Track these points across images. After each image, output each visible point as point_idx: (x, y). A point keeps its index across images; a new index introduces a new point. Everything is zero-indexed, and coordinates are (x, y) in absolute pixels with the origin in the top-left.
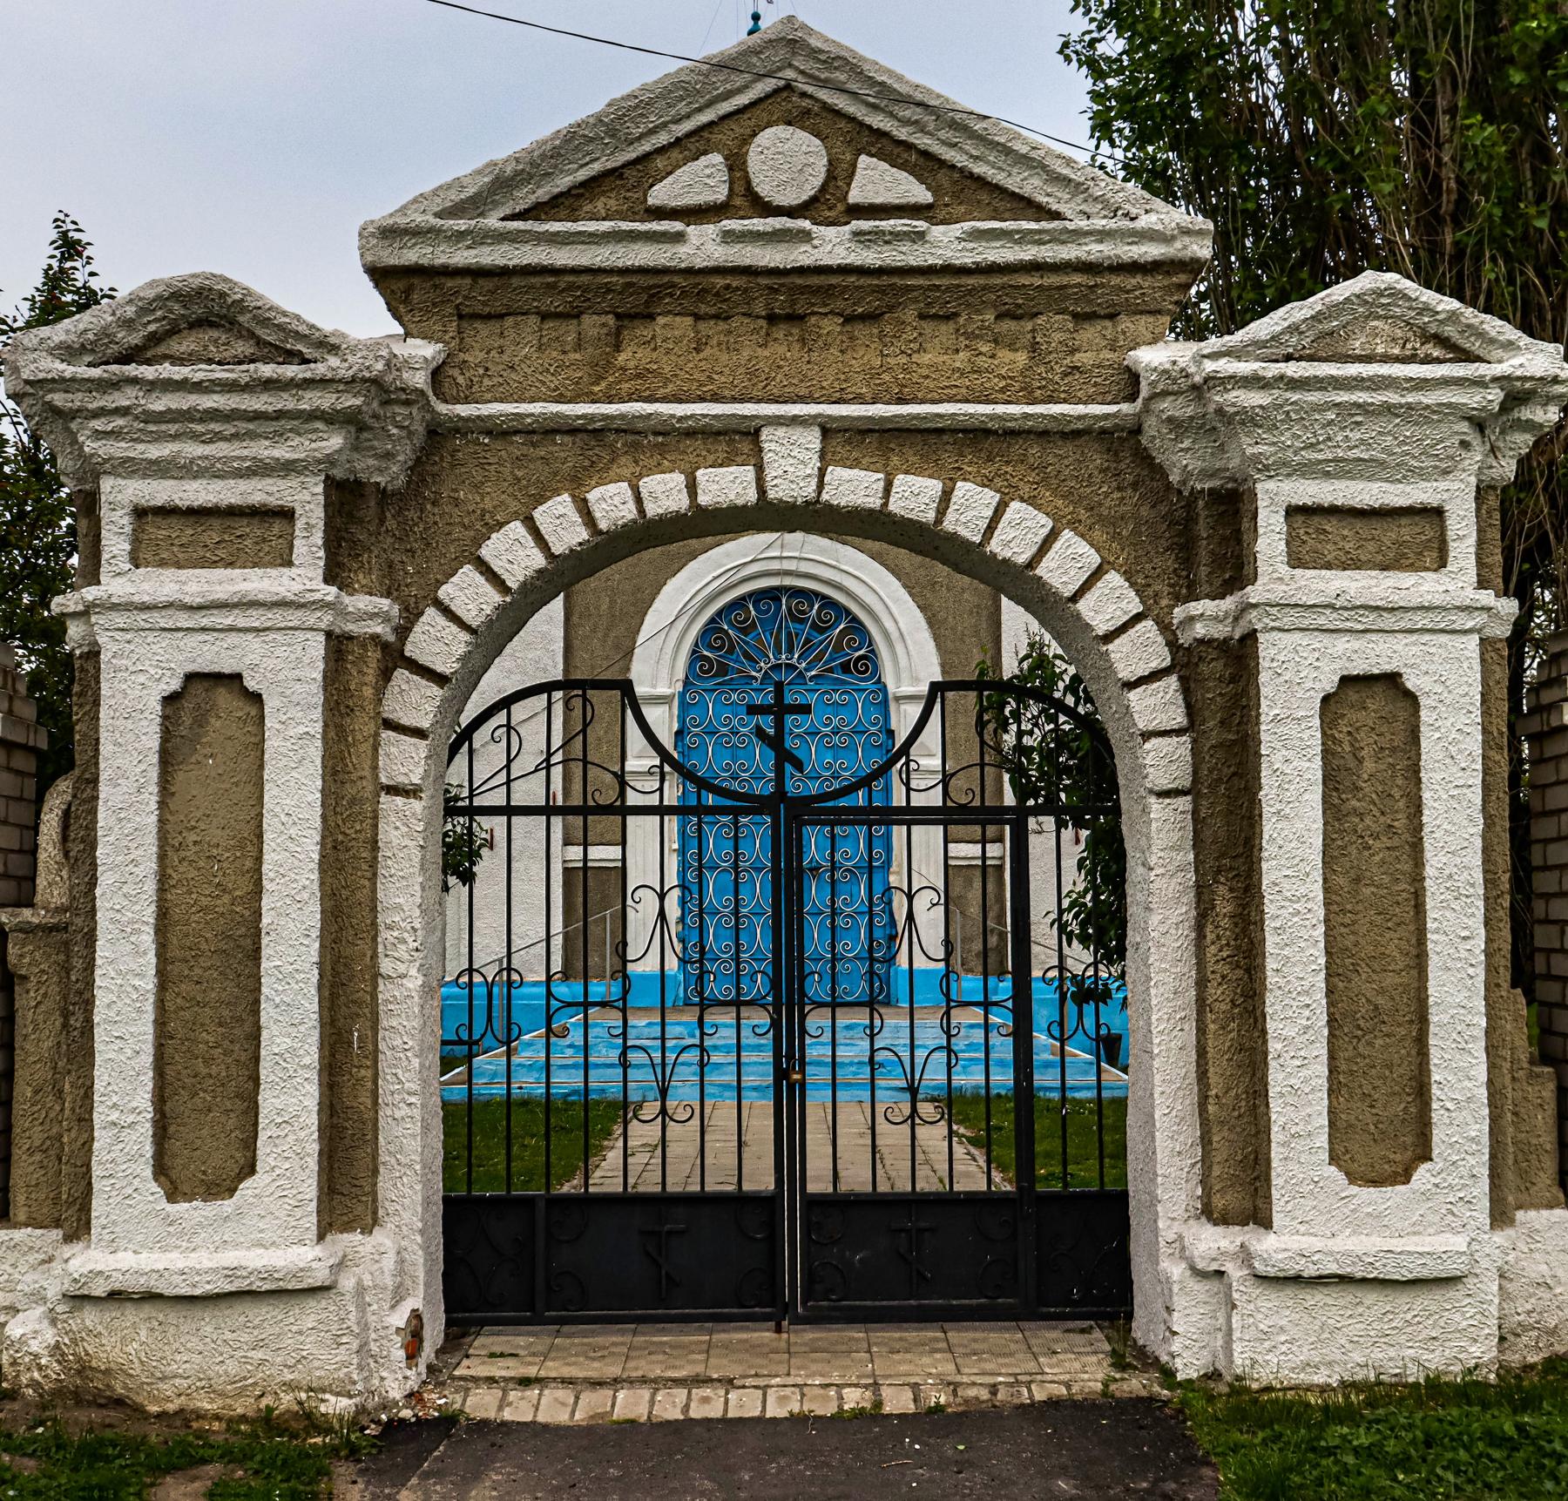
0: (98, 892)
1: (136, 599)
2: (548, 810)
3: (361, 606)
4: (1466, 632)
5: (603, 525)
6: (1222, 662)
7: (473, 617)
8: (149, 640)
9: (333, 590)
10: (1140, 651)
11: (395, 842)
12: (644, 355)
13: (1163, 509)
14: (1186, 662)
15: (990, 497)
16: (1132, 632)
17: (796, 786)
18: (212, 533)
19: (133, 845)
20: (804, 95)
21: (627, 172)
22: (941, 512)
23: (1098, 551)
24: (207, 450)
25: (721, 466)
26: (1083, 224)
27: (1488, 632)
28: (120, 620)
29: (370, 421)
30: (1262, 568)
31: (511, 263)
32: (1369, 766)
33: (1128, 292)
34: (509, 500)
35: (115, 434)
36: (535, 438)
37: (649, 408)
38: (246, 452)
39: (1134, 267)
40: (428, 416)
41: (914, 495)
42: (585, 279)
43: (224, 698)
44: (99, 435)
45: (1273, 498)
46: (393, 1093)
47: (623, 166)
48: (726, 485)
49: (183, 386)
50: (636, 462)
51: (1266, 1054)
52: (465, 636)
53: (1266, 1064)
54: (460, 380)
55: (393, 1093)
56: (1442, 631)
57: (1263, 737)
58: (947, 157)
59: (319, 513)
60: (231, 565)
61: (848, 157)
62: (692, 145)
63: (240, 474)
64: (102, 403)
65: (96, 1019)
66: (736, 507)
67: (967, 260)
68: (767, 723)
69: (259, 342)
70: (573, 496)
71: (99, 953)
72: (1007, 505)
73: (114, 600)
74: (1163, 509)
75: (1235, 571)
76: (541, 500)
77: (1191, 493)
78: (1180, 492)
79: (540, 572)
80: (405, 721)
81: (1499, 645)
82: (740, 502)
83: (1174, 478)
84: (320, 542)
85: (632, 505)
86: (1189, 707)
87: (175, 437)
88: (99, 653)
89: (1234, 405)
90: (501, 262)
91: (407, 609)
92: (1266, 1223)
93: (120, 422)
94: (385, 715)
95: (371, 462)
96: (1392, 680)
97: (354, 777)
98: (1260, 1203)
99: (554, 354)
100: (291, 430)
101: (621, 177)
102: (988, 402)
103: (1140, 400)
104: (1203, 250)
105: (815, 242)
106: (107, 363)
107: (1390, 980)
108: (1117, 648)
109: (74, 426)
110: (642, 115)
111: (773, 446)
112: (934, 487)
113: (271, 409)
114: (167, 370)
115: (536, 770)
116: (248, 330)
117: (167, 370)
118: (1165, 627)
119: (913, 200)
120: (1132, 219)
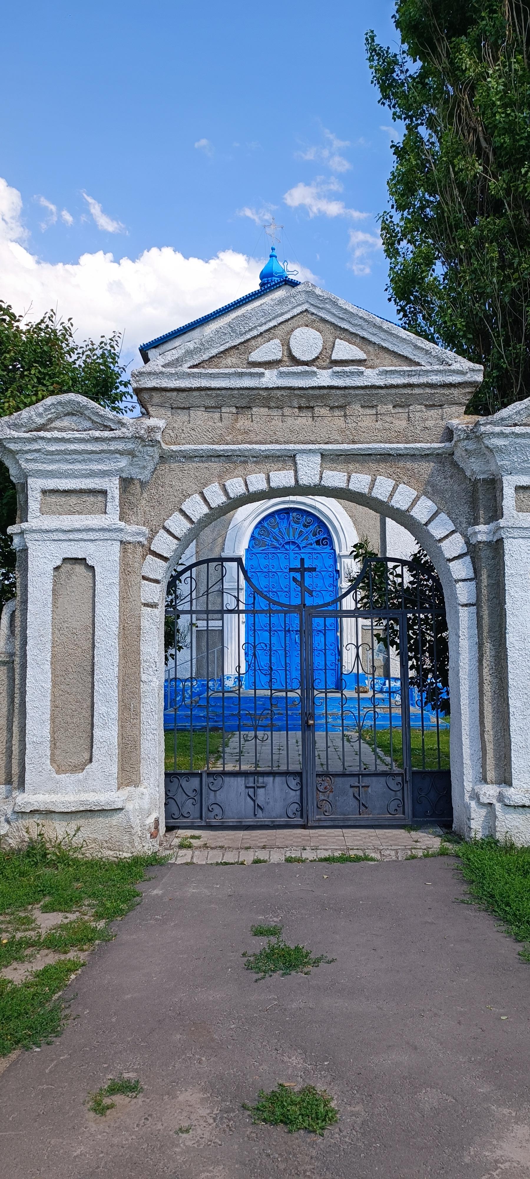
0: (27, 648)
1: (43, 528)
3: (134, 530)
5: (232, 495)
6: (489, 551)
8: (48, 544)
9: (123, 523)
10: (454, 546)
13: (463, 486)
14: (472, 550)
15: (391, 483)
16: (450, 538)
17: (309, 601)
18: (73, 500)
19: (41, 629)
20: (313, 314)
21: (240, 347)
22: (371, 489)
23: (436, 504)
24: (71, 467)
25: (279, 470)
26: (429, 368)
28: (36, 536)
29: (137, 453)
30: (505, 512)
31: (193, 386)
33: (448, 396)
34: (193, 486)
35: (34, 460)
36: (204, 459)
37: (250, 447)
38: (87, 467)
39: (451, 385)
40: (160, 451)
41: (360, 482)
42: (223, 392)
43: (80, 569)
46: (146, 729)
47: (239, 344)
49: (63, 440)
50: (245, 469)
51: (509, 713)
53: (509, 717)
54: (172, 434)
55: (146, 729)
57: (506, 582)
58: (373, 340)
59: (117, 492)
60: (80, 513)
61: (331, 339)
62: (267, 334)
63: (86, 476)
64: (29, 448)
65: (27, 700)
66: (286, 487)
67: (381, 383)
68: (298, 576)
69: (93, 422)
70: (219, 483)
71: (28, 673)
72: (398, 486)
73: (34, 528)
74: (463, 486)
75: (495, 513)
76: (205, 485)
77: (475, 480)
78: (470, 479)
79: (206, 515)
80: (151, 577)
82: (288, 485)
83: (468, 474)
84: (118, 504)
85: (244, 487)
86: (475, 569)
87: (58, 461)
88: (27, 549)
89: (493, 444)
90: (190, 386)
91: (151, 530)
92: (510, 785)
93: (37, 455)
94: (143, 574)
95: (137, 470)
97: (131, 600)
98: (506, 775)
99: (210, 423)
100: (106, 458)
101: (238, 349)
103: (453, 442)
105: (318, 376)
106: (32, 431)
108: (444, 545)
109: (17, 457)
110: (246, 323)
111: (301, 462)
112: (368, 478)
113: (98, 449)
114: (56, 434)
115: (203, 596)
116: (88, 417)
117: (56, 434)
118: (465, 536)
119: (358, 358)
120: (450, 365)
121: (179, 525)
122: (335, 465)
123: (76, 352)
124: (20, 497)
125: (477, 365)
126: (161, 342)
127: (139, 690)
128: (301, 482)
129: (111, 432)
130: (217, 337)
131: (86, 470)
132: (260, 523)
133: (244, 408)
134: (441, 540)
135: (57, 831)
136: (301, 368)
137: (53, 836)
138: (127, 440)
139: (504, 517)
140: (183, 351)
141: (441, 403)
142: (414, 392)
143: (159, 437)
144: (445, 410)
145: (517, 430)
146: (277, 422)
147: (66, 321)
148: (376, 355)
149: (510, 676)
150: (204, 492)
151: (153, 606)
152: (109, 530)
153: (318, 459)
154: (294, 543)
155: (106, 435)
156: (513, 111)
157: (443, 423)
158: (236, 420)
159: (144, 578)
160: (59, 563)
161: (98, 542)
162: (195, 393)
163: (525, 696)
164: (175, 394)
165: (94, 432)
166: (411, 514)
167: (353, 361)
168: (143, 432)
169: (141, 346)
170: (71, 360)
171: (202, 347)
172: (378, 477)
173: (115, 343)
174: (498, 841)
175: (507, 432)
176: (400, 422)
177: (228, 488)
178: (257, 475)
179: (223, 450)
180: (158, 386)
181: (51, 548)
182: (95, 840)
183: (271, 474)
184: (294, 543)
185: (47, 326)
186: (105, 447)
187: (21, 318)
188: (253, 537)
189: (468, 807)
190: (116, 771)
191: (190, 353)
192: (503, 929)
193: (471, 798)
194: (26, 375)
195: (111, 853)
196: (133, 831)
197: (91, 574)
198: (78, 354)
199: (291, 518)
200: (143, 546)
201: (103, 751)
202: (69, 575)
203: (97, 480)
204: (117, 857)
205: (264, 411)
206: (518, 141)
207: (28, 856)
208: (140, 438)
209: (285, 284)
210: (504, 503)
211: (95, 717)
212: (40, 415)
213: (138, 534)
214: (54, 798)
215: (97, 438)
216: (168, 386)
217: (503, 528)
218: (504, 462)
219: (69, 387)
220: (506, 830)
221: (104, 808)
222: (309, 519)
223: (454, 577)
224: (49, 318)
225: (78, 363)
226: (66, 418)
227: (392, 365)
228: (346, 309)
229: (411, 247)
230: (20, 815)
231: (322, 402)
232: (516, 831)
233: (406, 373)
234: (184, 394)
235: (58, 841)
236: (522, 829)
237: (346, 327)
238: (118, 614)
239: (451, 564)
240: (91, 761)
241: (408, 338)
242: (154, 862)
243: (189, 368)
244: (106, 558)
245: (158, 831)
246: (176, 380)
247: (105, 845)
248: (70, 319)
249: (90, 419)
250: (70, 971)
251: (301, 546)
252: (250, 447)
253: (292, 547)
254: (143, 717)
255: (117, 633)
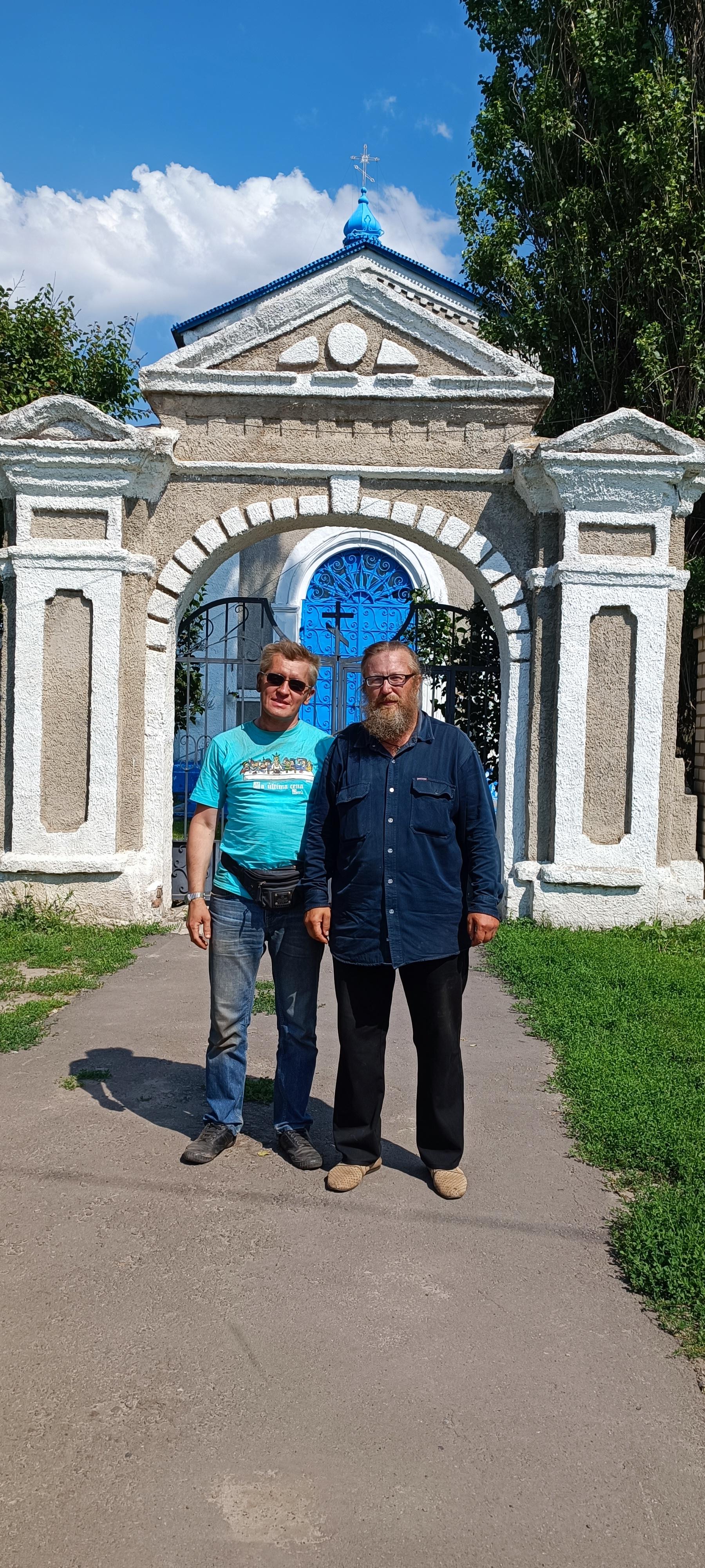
0: (15, 690)
2: (225, 661)
3: (138, 559)
4: (661, 587)
5: (254, 523)
7: (191, 566)
10: (508, 591)
11: (153, 672)
12: (276, 437)
16: (505, 582)
18: (69, 522)
19: (31, 669)
20: (357, 307)
26: (490, 378)
27: (673, 587)
30: (566, 552)
32: (612, 649)
34: (210, 509)
35: (24, 474)
43: (76, 602)
44: (16, 474)
45: (573, 520)
47: (268, 342)
48: (314, 503)
52: (188, 575)
54: (187, 448)
56: (651, 586)
57: (562, 634)
60: (76, 537)
61: (378, 339)
65: (14, 748)
66: (318, 515)
68: (332, 621)
69: (92, 430)
73: (23, 553)
75: (555, 554)
76: (224, 509)
80: (159, 615)
81: (680, 593)
83: (530, 507)
84: (120, 528)
85: (268, 513)
91: (160, 561)
94: (149, 612)
96: (624, 610)
101: (266, 347)
102: (442, 467)
104: (550, 393)
105: (360, 384)
106: (20, 438)
107: (616, 750)
108: (497, 589)
110: (277, 316)
112: (414, 508)
114: (49, 443)
117: (49, 443)
119: (408, 363)
121: (192, 557)
122: (376, 491)
123: (79, 339)
124: (7, 516)
125: (547, 377)
126: (201, 322)
127: (142, 744)
128: (335, 510)
129: (113, 443)
130: (242, 331)
131: (84, 487)
132: (322, 566)
133: (272, 419)
134: (494, 584)
135: (48, 894)
136: (338, 374)
137: (42, 899)
138: (131, 453)
139: (564, 559)
140: (201, 347)
141: (503, 422)
142: (471, 407)
143: (168, 450)
144: (507, 430)
145: (583, 456)
146: (311, 438)
147: (66, 301)
148: (430, 360)
149: (559, 741)
150: (222, 517)
151: (160, 649)
152: (110, 559)
153: (356, 483)
154: (364, 594)
155: (107, 447)
156: (616, 54)
157: (506, 446)
158: (262, 434)
159: (150, 616)
160: (51, 594)
161: (96, 572)
162: (215, 400)
163: (575, 764)
164: (190, 399)
165: (92, 441)
166: (461, 552)
167: (402, 366)
168: (149, 444)
169: (174, 327)
170: (73, 349)
171: (223, 343)
172: (426, 507)
173: (127, 331)
174: (535, 922)
175: (571, 458)
176: (455, 443)
177: (250, 513)
178: (284, 499)
179: (246, 469)
180: (171, 389)
181: (43, 577)
182: (89, 906)
183: (300, 498)
184: (364, 594)
185: (43, 305)
186: (106, 460)
187: (10, 292)
188: (312, 585)
189: (507, 885)
190: (114, 831)
191: (209, 351)
192: (507, 989)
193: (510, 876)
194: (15, 369)
195: (108, 920)
196: (132, 898)
197: (88, 609)
198: (81, 341)
199: (362, 561)
200: (149, 579)
201: (100, 808)
202: (63, 611)
203: (96, 500)
204: (114, 925)
205: (295, 424)
206: (621, 92)
207: (16, 919)
208: (146, 450)
209: (366, 248)
210: (565, 542)
211: (91, 771)
212: (30, 419)
213: (144, 564)
214: (43, 858)
215: (97, 449)
216: (183, 389)
217: (562, 571)
218: (567, 495)
219: (69, 385)
220: (544, 908)
221: (102, 871)
222: (387, 564)
223: (507, 628)
224: (45, 294)
225: (81, 353)
226: (61, 424)
227: (448, 374)
228: (396, 303)
229: (493, 220)
230: (6, 875)
231: (364, 415)
232: (555, 910)
233: (463, 385)
234: (202, 400)
235: (48, 906)
236: (561, 908)
237: (396, 324)
238: (118, 656)
239: (504, 613)
240: (86, 819)
241: (468, 341)
242: (154, 930)
243: (208, 368)
244: (105, 590)
245: (162, 900)
246: (191, 383)
247: (101, 911)
248: (71, 297)
249: (89, 426)
250: (54, 1007)
251: (374, 598)
252: (277, 465)
253: (362, 599)
254: (147, 774)
255: (117, 677)
